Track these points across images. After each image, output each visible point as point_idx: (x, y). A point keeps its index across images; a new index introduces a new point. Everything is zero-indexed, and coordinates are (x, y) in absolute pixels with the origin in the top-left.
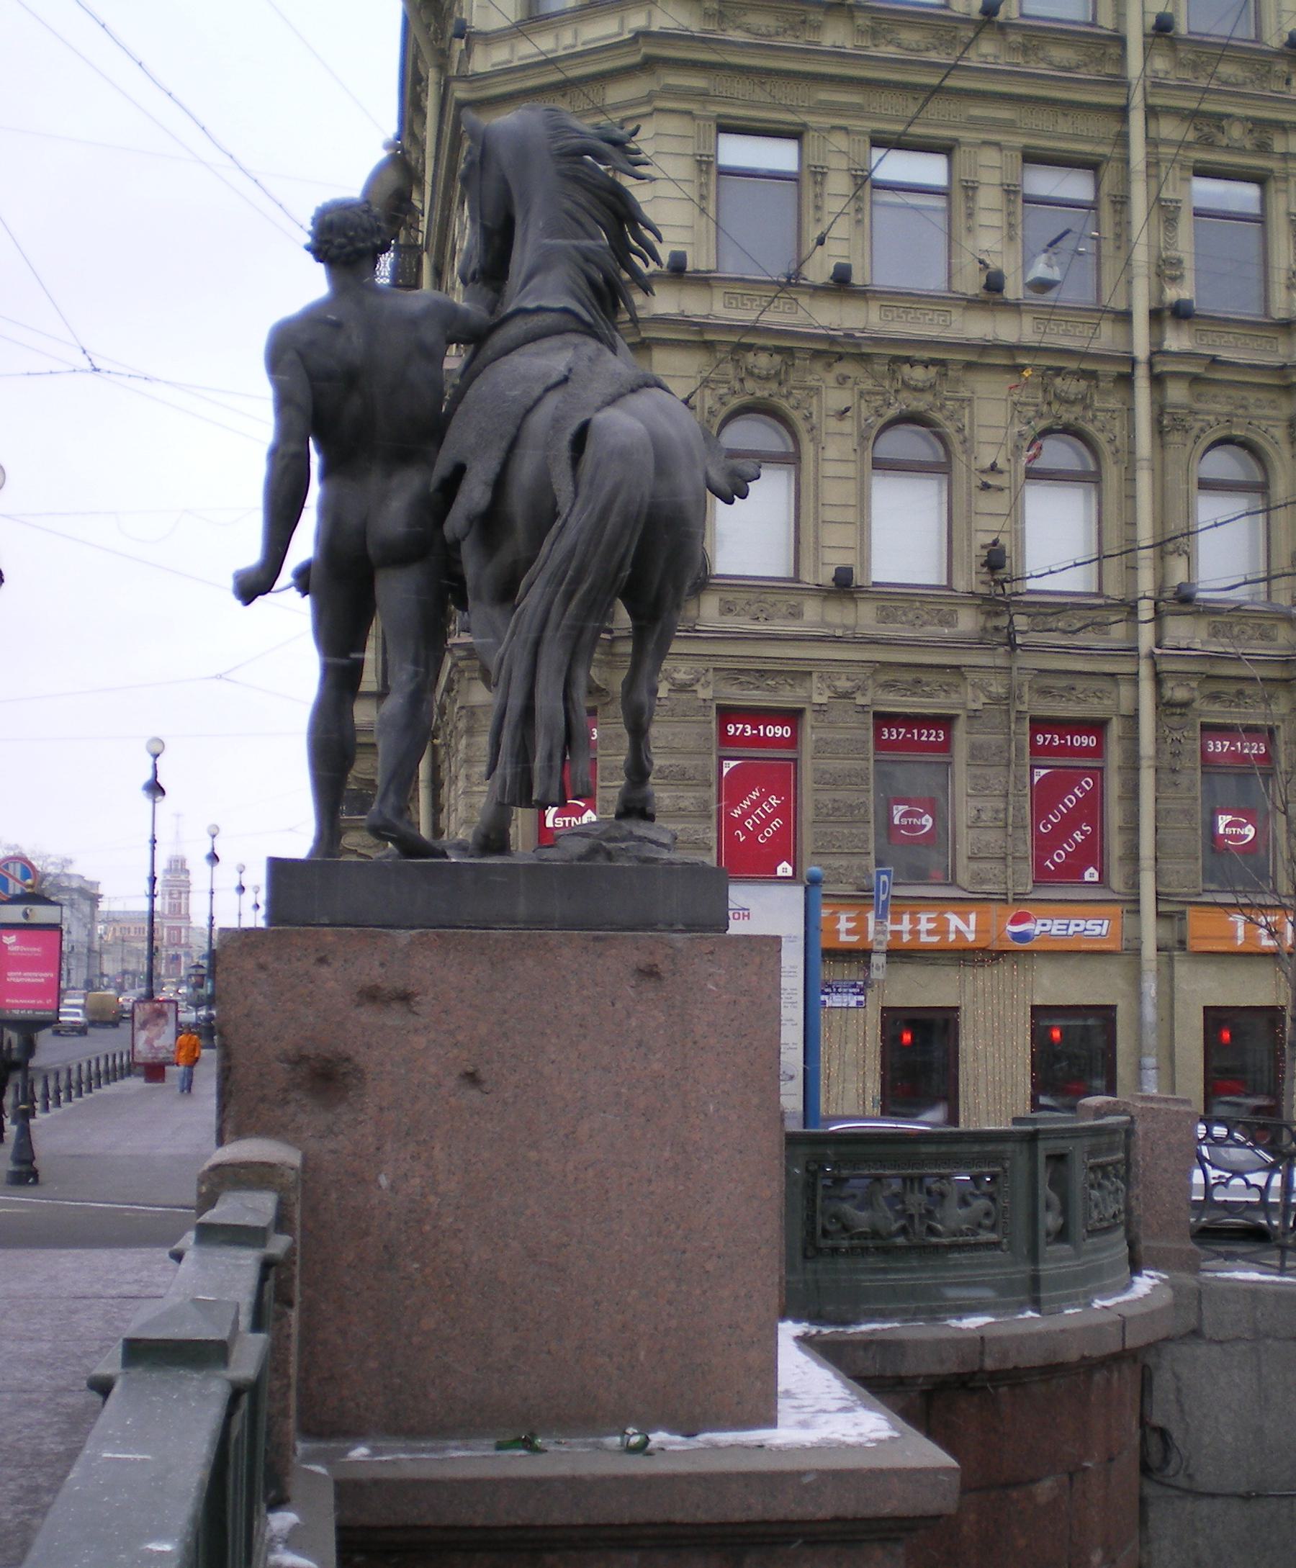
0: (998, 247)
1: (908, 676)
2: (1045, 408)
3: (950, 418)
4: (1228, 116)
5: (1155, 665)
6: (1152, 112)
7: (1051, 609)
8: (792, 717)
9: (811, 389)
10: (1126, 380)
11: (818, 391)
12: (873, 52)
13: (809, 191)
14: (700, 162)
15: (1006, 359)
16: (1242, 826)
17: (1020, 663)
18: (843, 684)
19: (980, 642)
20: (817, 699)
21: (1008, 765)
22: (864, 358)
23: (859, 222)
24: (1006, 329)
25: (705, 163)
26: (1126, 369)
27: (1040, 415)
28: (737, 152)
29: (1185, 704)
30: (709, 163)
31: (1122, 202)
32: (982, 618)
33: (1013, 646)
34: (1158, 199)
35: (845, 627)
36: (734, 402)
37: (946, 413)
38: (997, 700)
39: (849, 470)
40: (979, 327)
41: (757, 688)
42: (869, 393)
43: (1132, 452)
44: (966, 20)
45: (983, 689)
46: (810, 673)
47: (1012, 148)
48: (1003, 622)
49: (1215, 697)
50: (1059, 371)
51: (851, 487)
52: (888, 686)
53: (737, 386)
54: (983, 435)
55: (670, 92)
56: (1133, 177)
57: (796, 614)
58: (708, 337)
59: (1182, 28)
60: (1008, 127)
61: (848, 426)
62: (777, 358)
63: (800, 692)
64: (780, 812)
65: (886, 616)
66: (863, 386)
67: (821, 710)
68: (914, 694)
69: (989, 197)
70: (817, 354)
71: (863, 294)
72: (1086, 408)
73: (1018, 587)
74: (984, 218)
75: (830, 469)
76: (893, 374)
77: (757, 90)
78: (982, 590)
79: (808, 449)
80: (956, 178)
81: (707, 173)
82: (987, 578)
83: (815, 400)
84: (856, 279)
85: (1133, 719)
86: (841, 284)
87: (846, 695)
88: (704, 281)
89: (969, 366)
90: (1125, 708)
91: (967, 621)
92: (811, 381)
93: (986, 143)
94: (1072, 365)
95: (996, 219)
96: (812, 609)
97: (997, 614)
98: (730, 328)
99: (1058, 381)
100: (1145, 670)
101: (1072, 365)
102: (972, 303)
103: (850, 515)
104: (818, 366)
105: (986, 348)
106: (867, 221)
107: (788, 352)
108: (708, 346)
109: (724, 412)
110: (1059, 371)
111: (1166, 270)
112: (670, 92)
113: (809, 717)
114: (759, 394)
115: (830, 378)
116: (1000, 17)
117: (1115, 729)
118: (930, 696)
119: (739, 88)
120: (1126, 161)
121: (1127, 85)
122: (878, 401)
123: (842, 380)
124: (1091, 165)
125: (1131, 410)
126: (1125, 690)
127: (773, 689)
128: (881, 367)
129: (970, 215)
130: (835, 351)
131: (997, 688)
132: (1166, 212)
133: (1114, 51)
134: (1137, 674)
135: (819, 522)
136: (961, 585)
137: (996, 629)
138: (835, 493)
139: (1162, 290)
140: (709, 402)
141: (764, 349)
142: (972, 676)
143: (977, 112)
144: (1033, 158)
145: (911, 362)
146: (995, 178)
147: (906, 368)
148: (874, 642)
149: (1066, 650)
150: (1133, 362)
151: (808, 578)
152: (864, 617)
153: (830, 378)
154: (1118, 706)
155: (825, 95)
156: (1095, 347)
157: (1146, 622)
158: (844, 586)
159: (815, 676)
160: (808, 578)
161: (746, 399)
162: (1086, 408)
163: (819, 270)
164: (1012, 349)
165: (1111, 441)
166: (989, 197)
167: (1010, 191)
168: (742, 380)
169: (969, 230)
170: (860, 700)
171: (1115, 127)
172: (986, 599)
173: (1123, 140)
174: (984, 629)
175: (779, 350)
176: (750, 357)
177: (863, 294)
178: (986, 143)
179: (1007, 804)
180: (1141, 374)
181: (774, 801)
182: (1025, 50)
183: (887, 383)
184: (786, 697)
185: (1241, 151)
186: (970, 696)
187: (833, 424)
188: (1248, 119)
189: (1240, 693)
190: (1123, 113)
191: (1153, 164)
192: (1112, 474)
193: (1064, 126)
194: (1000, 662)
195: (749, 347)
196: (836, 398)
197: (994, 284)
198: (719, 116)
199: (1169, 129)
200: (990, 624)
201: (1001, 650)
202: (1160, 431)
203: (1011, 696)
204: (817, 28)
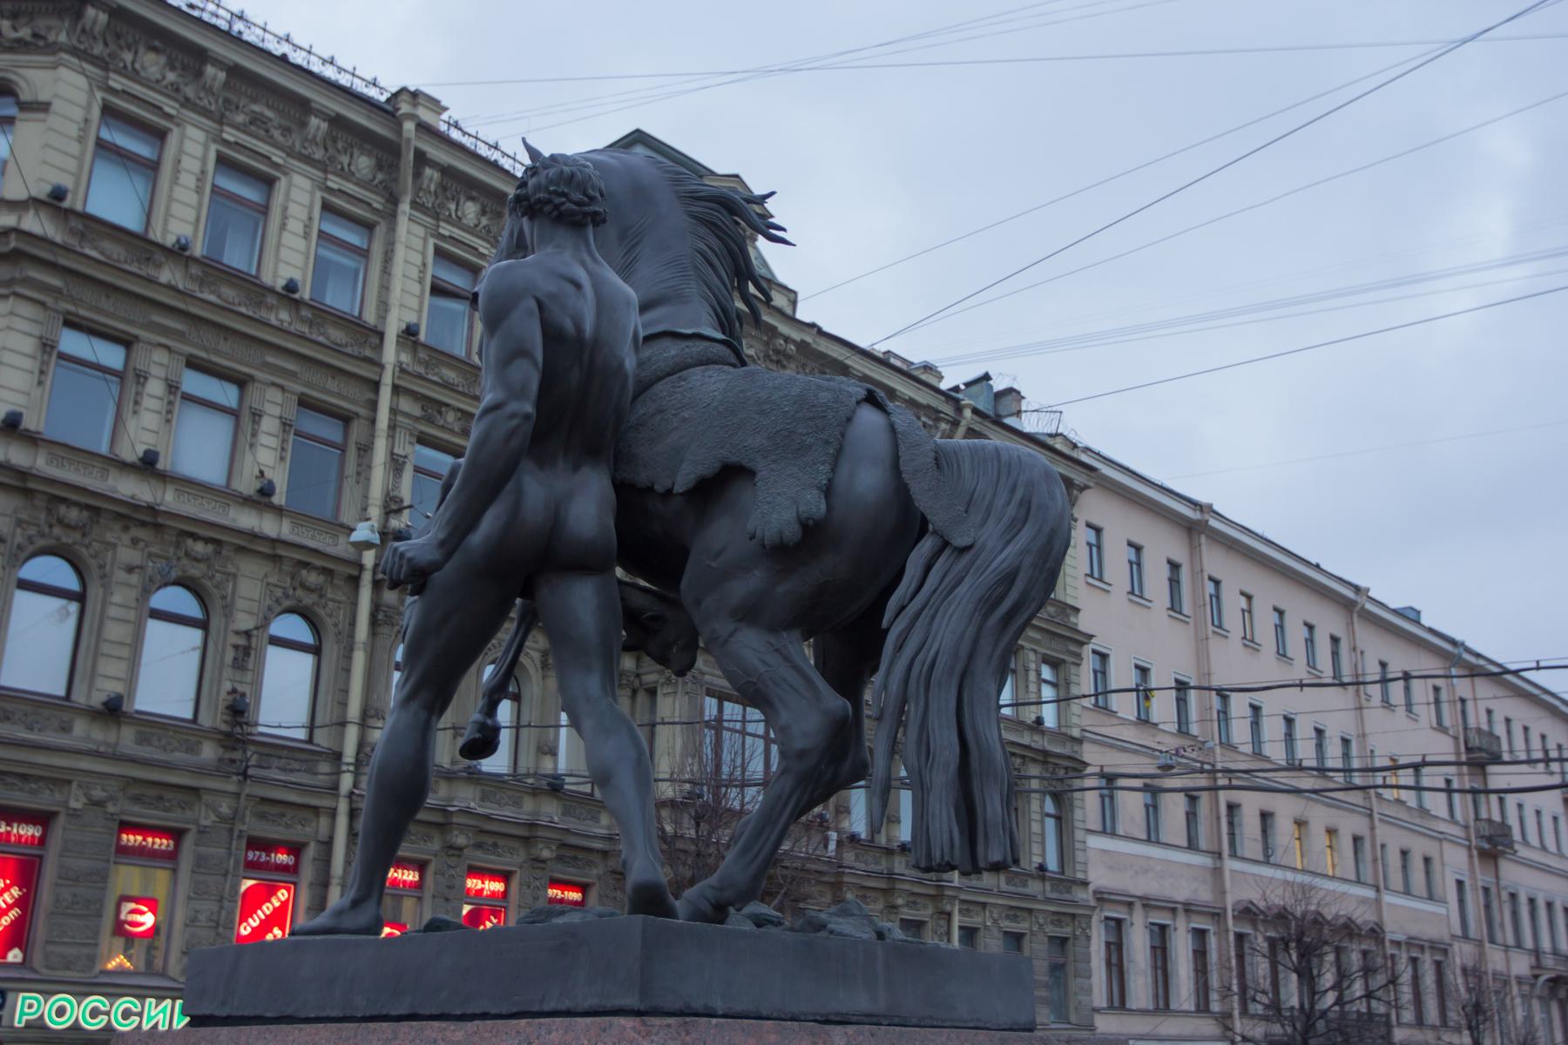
0: (271, 463)
1: (153, 792)
2: (291, 592)
3: (94, 557)
4: (447, 405)
5: (351, 802)
6: (396, 389)
7: (277, 750)
8: (43, 819)
9: (108, 544)
10: (355, 581)
11: (114, 546)
12: (199, 295)
13: (131, 389)
14: (45, 345)
15: (271, 551)
16: (142, 913)
17: (247, 790)
18: (98, 793)
19: (221, 769)
20: (74, 804)
21: (225, 875)
22: (158, 527)
23: (168, 421)
24: (269, 526)
25: (47, 346)
26: (355, 573)
27: (287, 596)
28: (74, 343)
29: (460, 849)
30: (52, 347)
31: (366, 449)
32: (221, 750)
33: (245, 775)
34: (392, 454)
35: (107, 744)
36: (41, 543)
37: (92, 551)
38: (222, 819)
39: (131, 615)
40: (246, 519)
41: (22, 790)
42: (157, 556)
43: (352, 635)
44: (271, 290)
45: (215, 810)
46: (69, 782)
47: (180, 354)
48: (237, 755)
49: (479, 846)
50: (306, 565)
51: (130, 628)
52: (137, 799)
53: (47, 530)
54: (240, 604)
55: (27, 281)
56: (378, 433)
57: (66, 728)
58: (31, 485)
59: (422, 337)
60: (179, 336)
61: (134, 579)
62: (85, 514)
63: (58, 796)
64: (18, 903)
65: (142, 740)
66: (153, 550)
67: (74, 814)
68: (157, 808)
69: (155, 387)
70: (119, 516)
71: (165, 478)
72: (321, 596)
73: (253, 730)
74: (264, 439)
75: (113, 611)
76: (178, 545)
77: (103, 299)
78: (224, 728)
79: (95, 593)
80: (247, 403)
81: (50, 355)
82: (228, 718)
83: (110, 554)
84: (160, 466)
85: (328, 844)
86: (147, 465)
87: (99, 804)
88: (33, 440)
89: (240, 549)
90: (323, 832)
91: (209, 752)
92: (110, 537)
93: (274, 384)
94: (318, 562)
95: (273, 442)
96: (80, 727)
97: (234, 749)
98: (53, 482)
99: (304, 572)
100: (343, 807)
101: (318, 562)
102: (246, 501)
103: (125, 652)
104: (117, 527)
105: (254, 536)
106: (48, 383)
107: (96, 511)
108: (28, 493)
109: (31, 548)
110: (306, 565)
111: (392, 506)
112: (27, 281)
113: (61, 821)
114: (64, 540)
115: (126, 538)
116: (66, 204)
117: (311, 852)
118: (166, 810)
119: (88, 294)
120: (373, 421)
121: (382, 367)
122: (32, 531)
123: (135, 542)
124: (346, 419)
125: (354, 604)
126: (324, 822)
127: (32, 792)
128: (287, 567)
129: (254, 435)
130: (148, 518)
131: (225, 809)
132: (396, 464)
133: (375, 340)
134: (335, 809)
135: (96, 654)
136: (206, 720)
137: (233, 761)
138: (114, 631)
139: (387, 520)
140: (19, 539)
141: (76, 504)
142: (206, 798)
143: (270, 359)
144: (194, 364)
145: (195, 537)
146: (277, 411)
147: (190, 542)
148: (133, 760)
149: (287, 785)
150: (361, 567)
151: (79, 697)
152: (126, 738)
153: (126, 538)
154: (317, 832)
155: (158, 318)
156: (330, 550)
157: (1508, 961)
158: (113, 711)
159: (74, 785)
160: (79, 697)
161: (52, 542)
162: (321, 596)
163: (247, 484)
164: (275, 542)
165: (336, 625)
166: (155, 387)
167: (172, 387)
168: (51, 526)
169: (252, 446)
170: (111, 808)
171: (370, 395)
172: (228, 735)
173: (373, 405)
174: (220, 760)
175: (88, 507)
176: (63, 509)
177: (165, 478)
178: (274, 384)
179: (221, 908)
180: (367, 578)
181: (15, 892)
182: (82, 236)
183: (172, 550)
184: (43, 800)
185: (452, 431)
186: (203, 813)
187: (121, 575)
188: (459, 410)
189: (495, 845)
190: (376, 386)
191: (392, 427)
192: (331, 649)
193: (332, 385)
194: (231, 788)
195: (64, 500)
196: (128, 555)
197: (266, 491)
198: (69, 313)
199: (405, 404)
200: (228, 755)
201: (235, 778)
202: (374, 622)
203: (231, 820)
204: (159, 266)
